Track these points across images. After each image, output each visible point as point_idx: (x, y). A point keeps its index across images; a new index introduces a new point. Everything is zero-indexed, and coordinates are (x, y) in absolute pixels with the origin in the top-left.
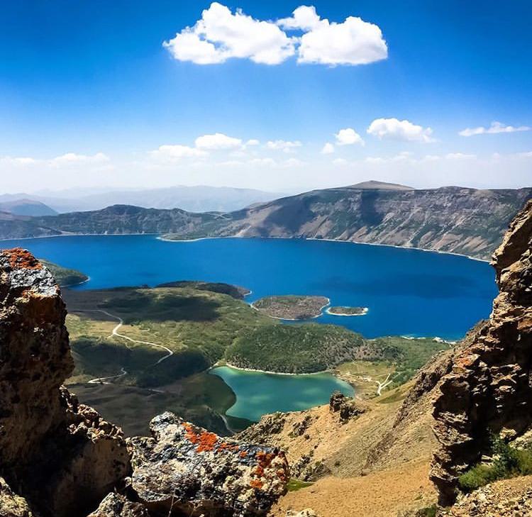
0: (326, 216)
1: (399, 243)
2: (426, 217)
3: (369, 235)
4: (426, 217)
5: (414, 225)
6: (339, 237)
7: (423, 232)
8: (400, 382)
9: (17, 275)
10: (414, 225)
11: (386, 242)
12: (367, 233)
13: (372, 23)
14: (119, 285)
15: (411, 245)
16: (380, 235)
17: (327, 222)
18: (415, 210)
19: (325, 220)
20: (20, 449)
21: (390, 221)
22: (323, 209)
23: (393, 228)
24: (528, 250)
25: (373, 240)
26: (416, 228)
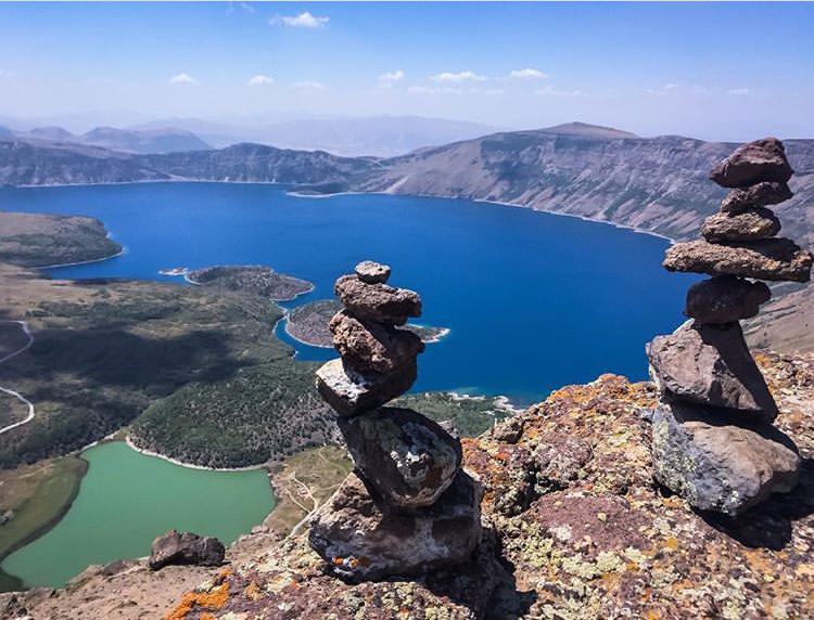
2: (632, 178)
3: (554, 200)
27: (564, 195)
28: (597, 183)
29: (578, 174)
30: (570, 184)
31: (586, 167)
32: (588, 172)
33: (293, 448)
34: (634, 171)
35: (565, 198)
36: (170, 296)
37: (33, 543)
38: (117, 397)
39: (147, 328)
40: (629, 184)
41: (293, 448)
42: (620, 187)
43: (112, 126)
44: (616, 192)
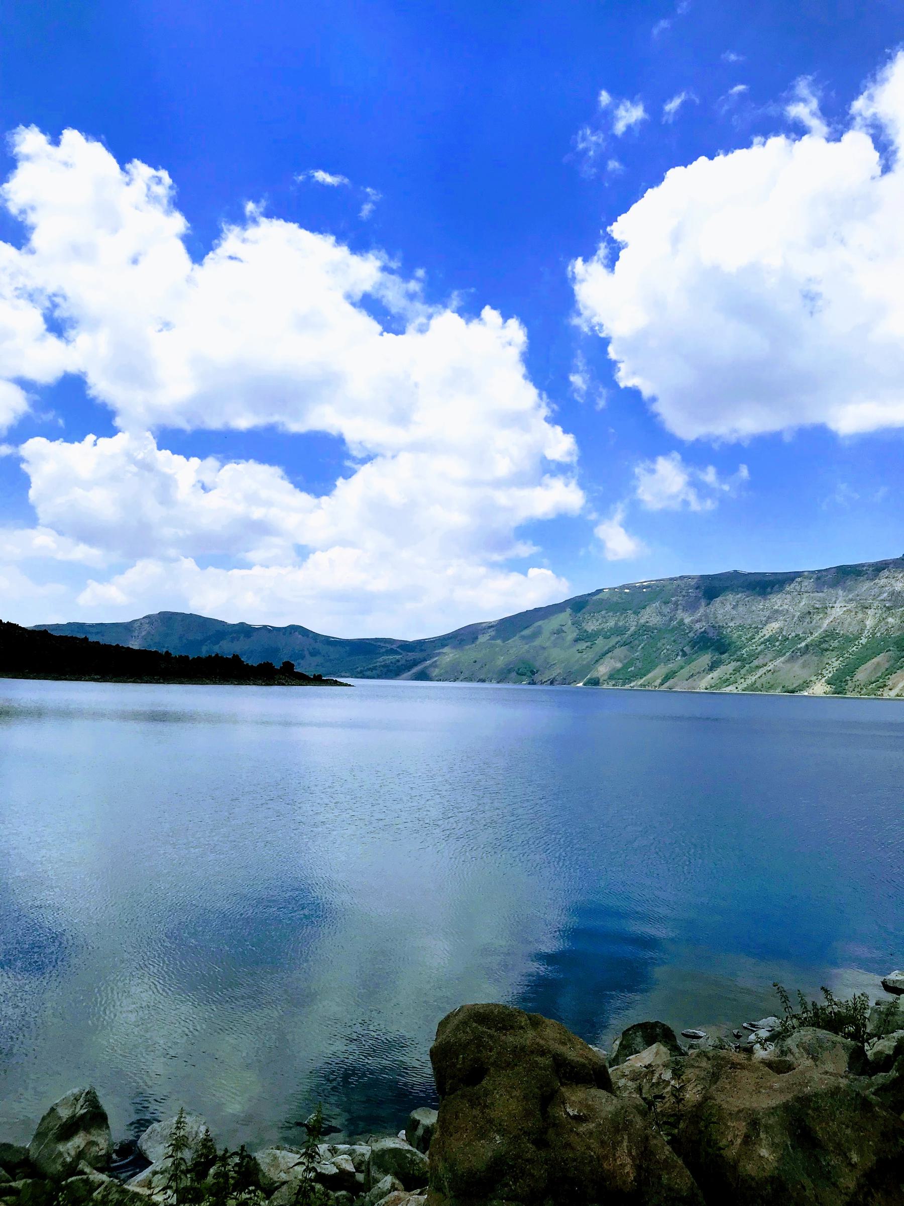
0: (614, 640)
1: (790, 688)
2: (869, 623)
3: (716, 674)
4: (869, 623)
5: (835, 644)
6: (641, 682)
7: (862, 659)
8: (636, 845)
9: (146, 889)
10: (835, 644)
11: (758, 685)
12: (712, 667)
13: (691, 163)
14: (160, 726)
15: (828, 688)
16: (743, 671)
17: (618, 652)
18: (838, 611)
19: (614, 647)
20: (66, 1109)
21: (771, 640)
22: (611, 623)
23: (780, 653)
24: (620, 128)
25: (726, 682)
26: (842, 649)
27: (734, 665)
28: (798, 638)
29: (757, 630)
30: (744, 646)
31: (769, 620)
32: (775, 626)
33: (83, 944)
34: (870, 612)
35: (736, 670)
36: (608, 681)
37: (31, 680)
38: (404, 309)
39: (395, 658)
40: (866, 633)
41: (83, 944)
42: (850, 640)
43: (469, 1002)
44: (842, 649)
